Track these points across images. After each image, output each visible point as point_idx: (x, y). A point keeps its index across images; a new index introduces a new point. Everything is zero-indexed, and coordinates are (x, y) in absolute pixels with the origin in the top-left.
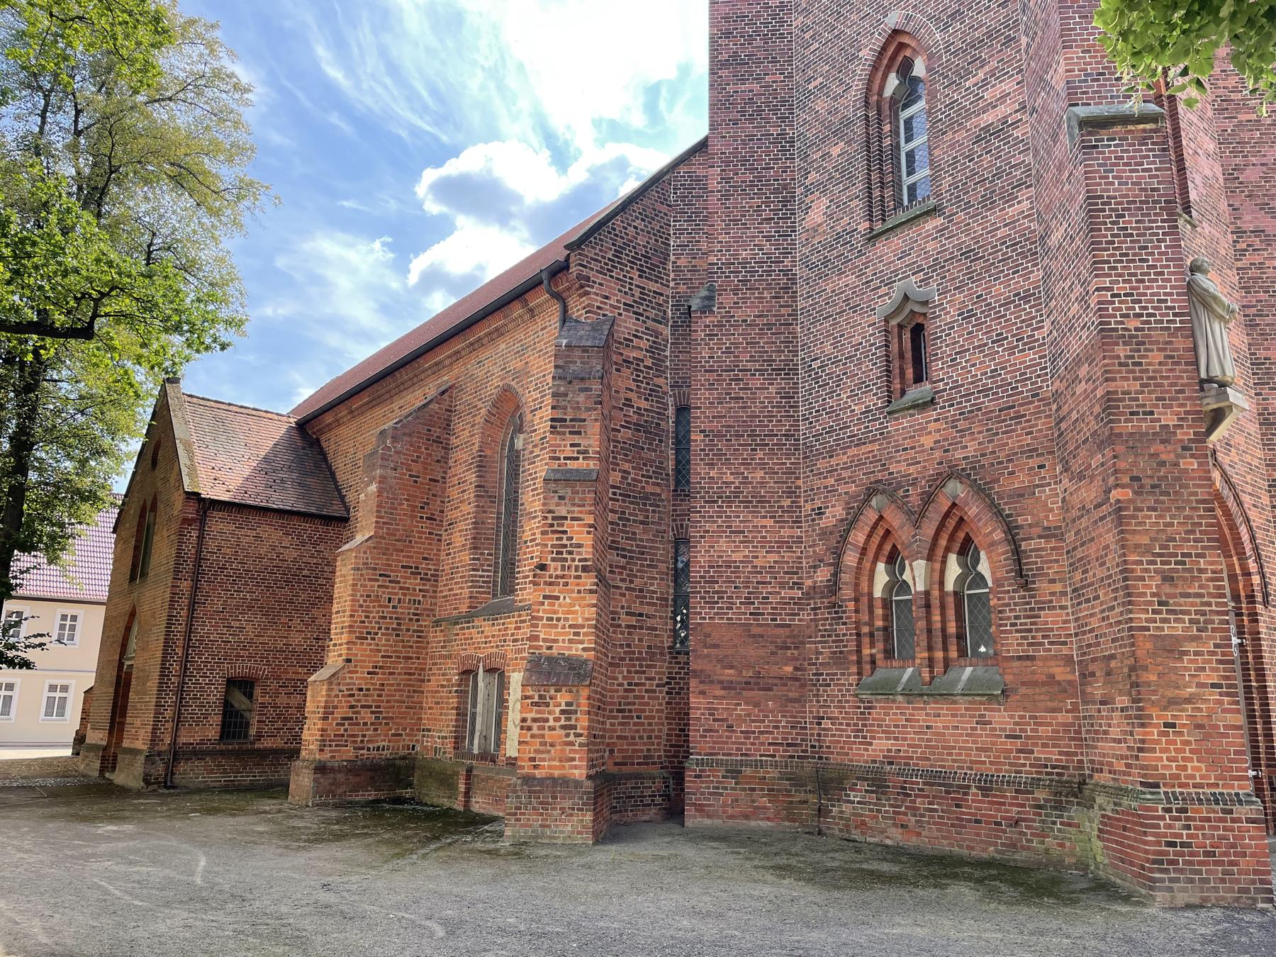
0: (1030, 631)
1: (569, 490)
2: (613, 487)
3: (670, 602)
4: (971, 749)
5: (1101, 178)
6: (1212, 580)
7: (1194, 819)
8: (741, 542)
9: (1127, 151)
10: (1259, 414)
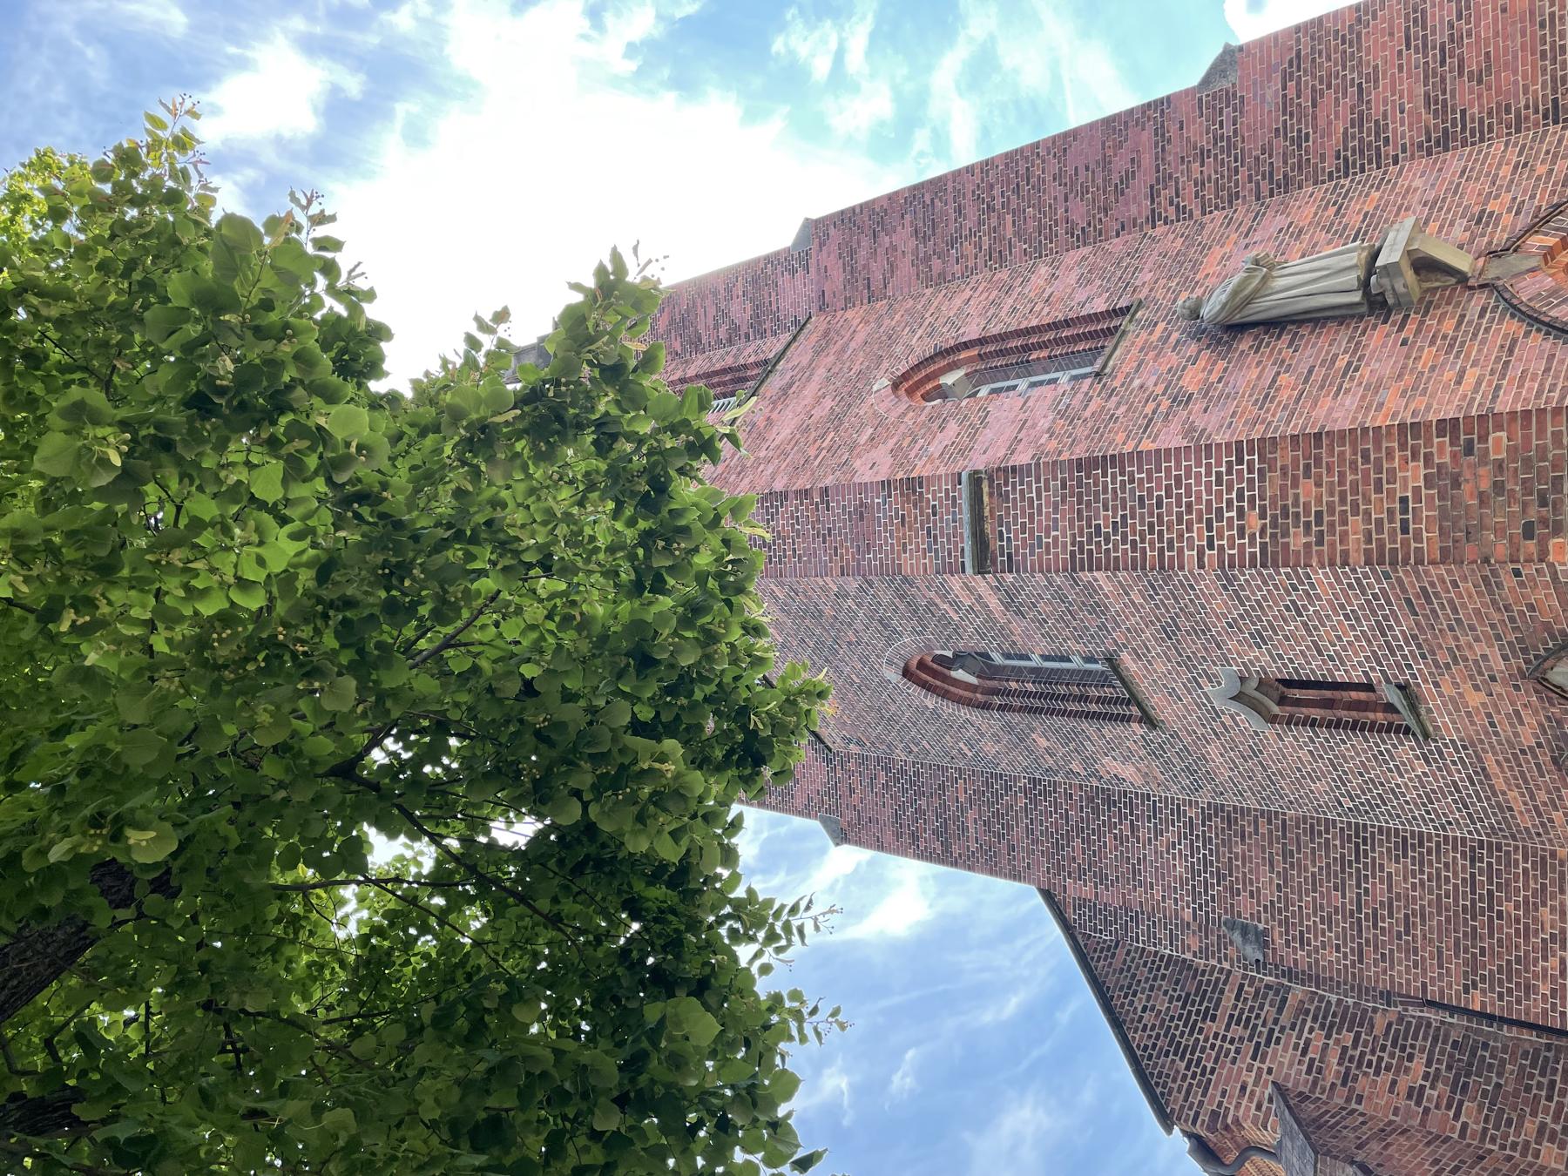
5: (1048, 553)
10: (1429, 154)
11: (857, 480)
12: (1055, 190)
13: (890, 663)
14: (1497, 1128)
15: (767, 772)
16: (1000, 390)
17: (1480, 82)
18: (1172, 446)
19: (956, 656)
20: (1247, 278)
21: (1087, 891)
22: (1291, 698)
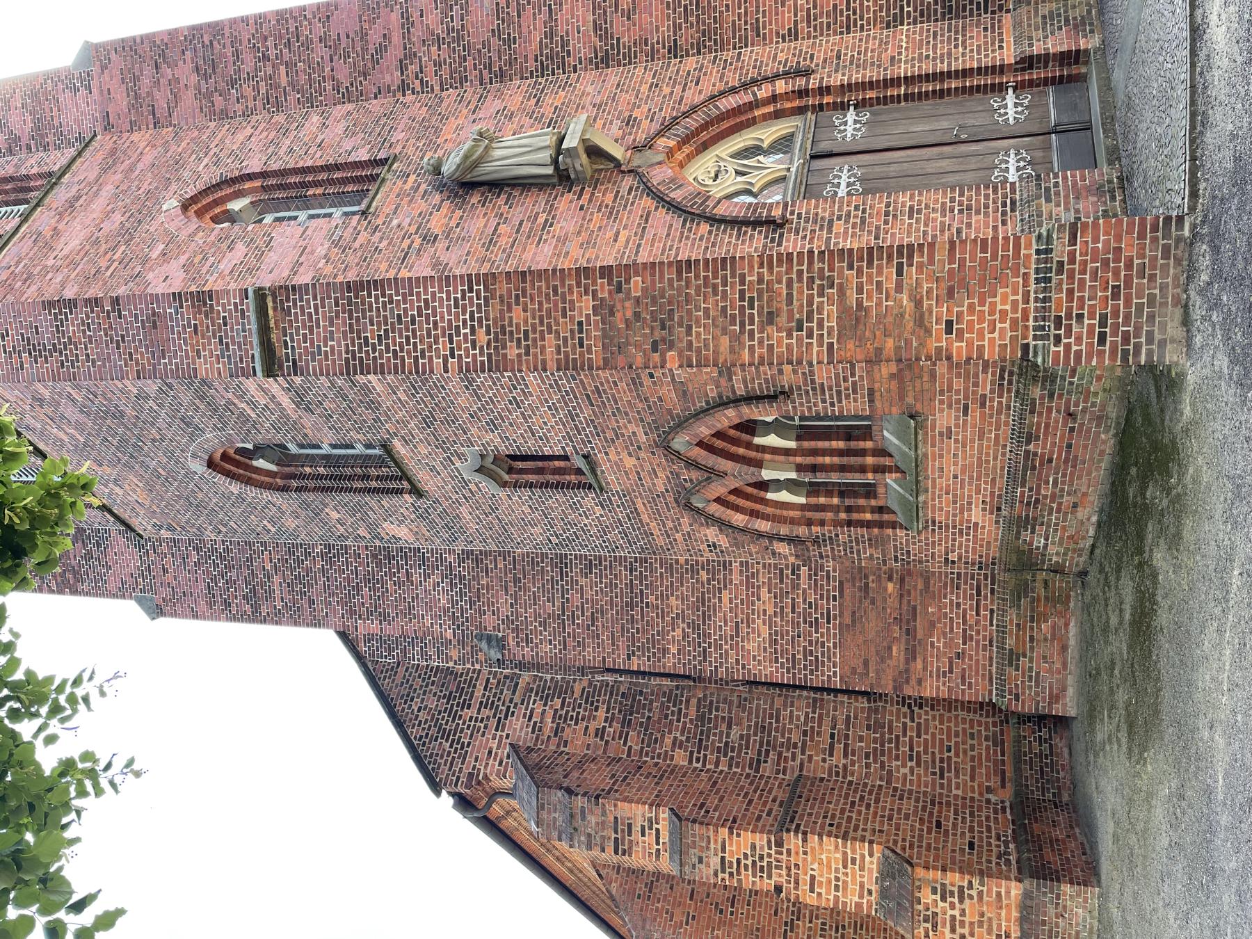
0: (839, 392)
1: (692, 851)
2: (690, 762)
3: (818, 696)
4: (981, 446)
5: (327, 360)
6: (771, 268)
7: (1070, 309)
8: (748, 627)
9: (297, 328)
10: (597, 68)
11: (149, 291)
12: (320, 51)
13: (194, 456)
14: (649, 746)
15: (31, 562)
16: (283, 219)
17: (629, 19)
18: (424, 274)
19: (257, 448)
20: (474, 146)
21: (374, 628)
22: (515, 468)
